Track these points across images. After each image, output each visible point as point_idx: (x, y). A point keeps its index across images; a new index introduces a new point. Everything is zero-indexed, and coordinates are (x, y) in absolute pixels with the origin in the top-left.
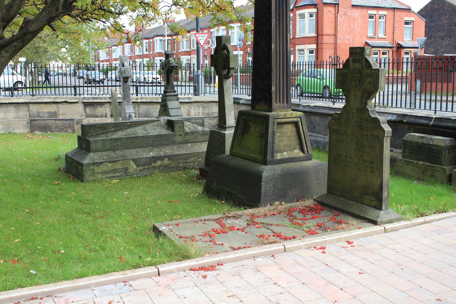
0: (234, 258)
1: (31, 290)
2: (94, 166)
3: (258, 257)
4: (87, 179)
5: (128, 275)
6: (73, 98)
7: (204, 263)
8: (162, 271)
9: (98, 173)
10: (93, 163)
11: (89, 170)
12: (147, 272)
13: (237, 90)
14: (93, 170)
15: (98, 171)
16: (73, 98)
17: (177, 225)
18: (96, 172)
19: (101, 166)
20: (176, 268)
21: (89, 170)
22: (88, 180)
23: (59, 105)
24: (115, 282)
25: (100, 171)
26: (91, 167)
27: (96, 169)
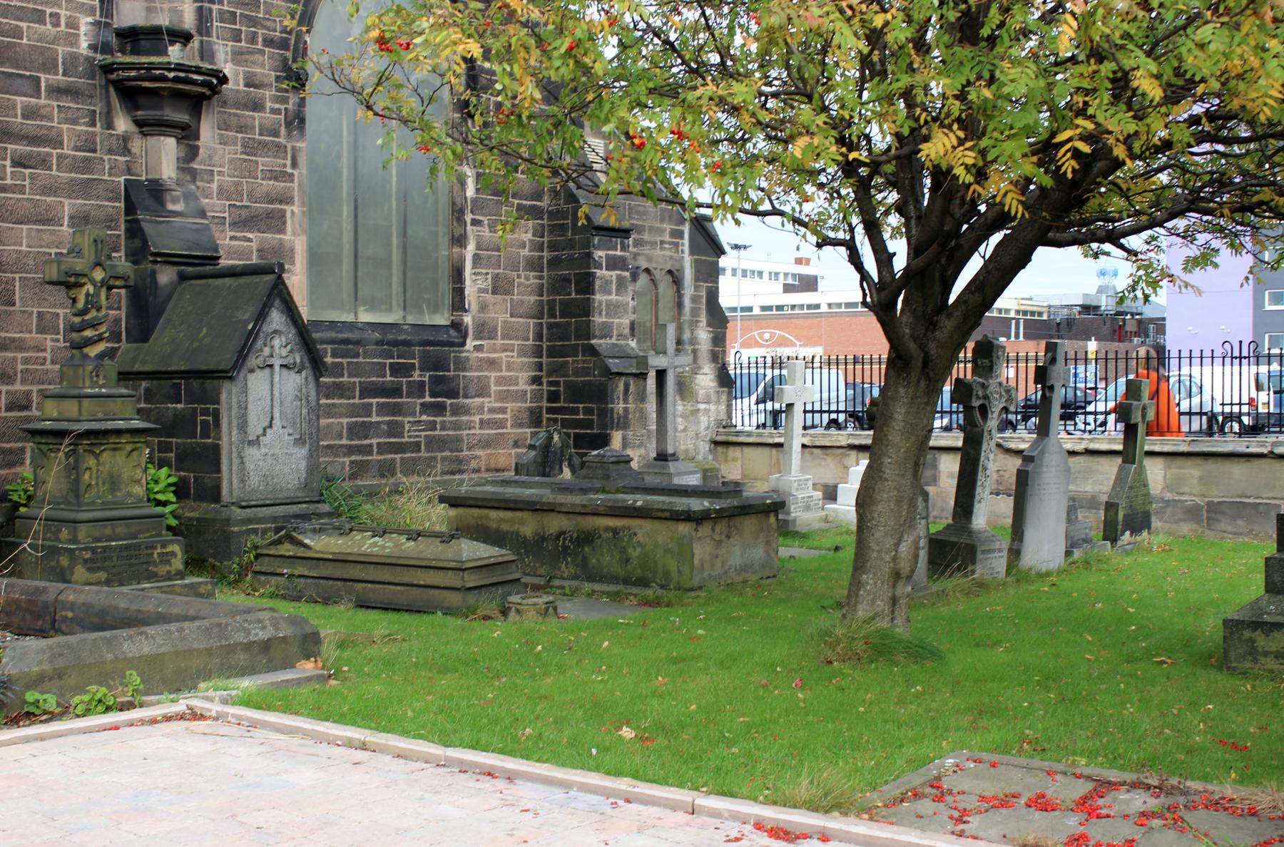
0: (864, 836)
1: (792, 814)
2: (1256, 630)
3: (382, 752)
4: (1233, 665)
5: (636, 790)
6: (771, 435)
7: (790, 822)
8: (700, 806)
9: (1266, 654)
10: (1252, 622)
11: (1239, 639)
12: (670, 796)
13: (850, 380)
14: (1252, 641)
15: (1267, 649)
16: (771, 435)
17: (994, 765)
18: (1260, 649)
19: (1276, 635)
20: (729, 811)
21: (1239, 639)
22: (1234, 669)
23: (747, 450)
24: (673, 806)
25: (1273, 649)
26: (1247, 634)
27: (1261, 640)
